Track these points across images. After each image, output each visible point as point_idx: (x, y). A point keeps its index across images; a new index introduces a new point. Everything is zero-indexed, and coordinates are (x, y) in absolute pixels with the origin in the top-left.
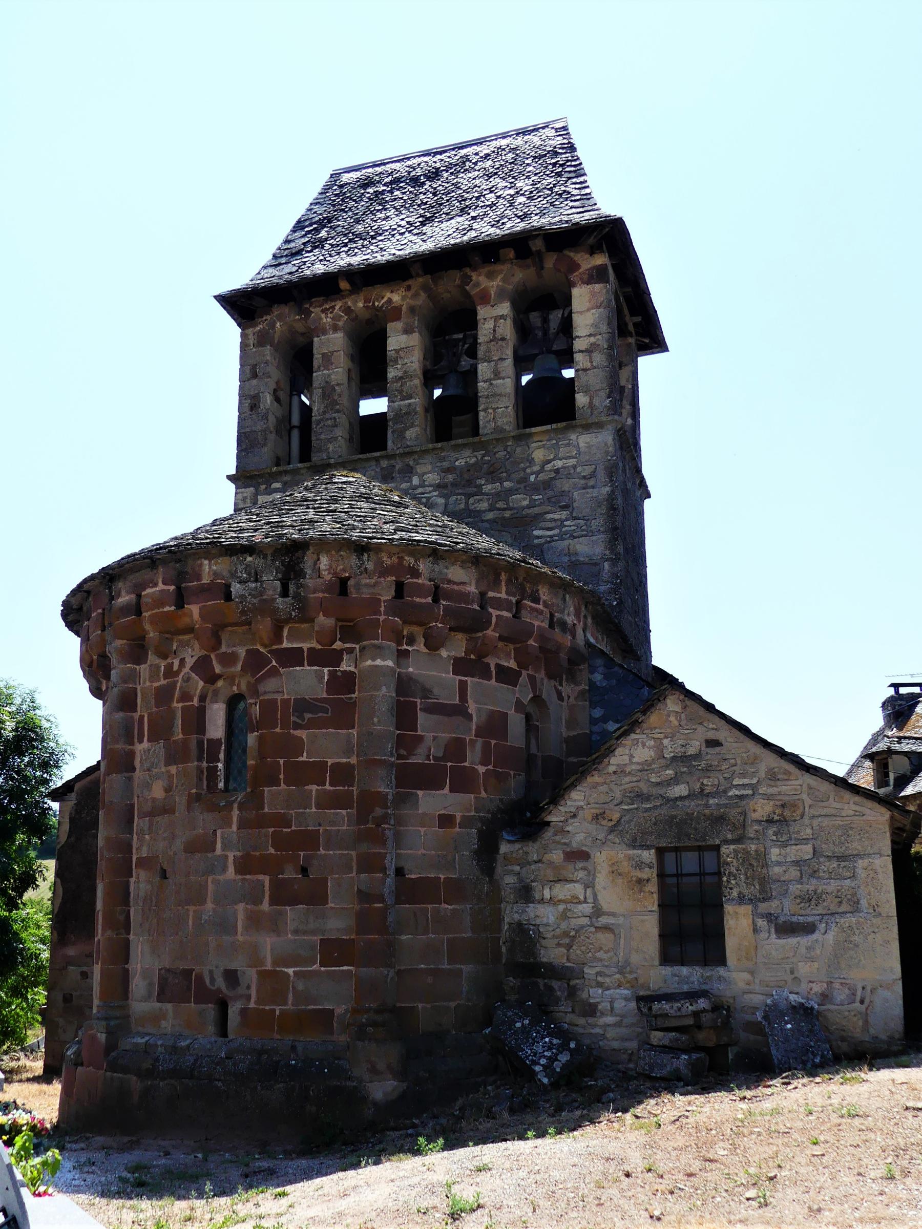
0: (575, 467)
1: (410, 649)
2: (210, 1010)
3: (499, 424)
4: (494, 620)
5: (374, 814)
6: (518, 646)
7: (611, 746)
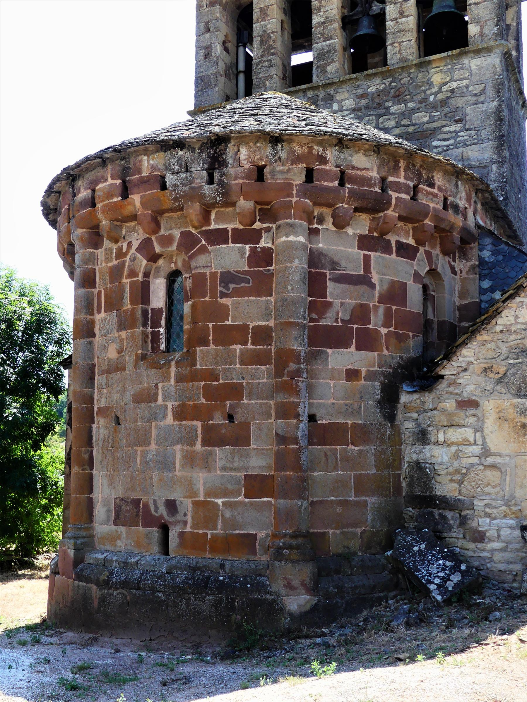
0: (467, 87)
1: (320, 227)
2: (155, 532)
3: (404, 55)
4: (394, 201)
5: (288, 369)
6: (415, 225)
7: (498, 309)
